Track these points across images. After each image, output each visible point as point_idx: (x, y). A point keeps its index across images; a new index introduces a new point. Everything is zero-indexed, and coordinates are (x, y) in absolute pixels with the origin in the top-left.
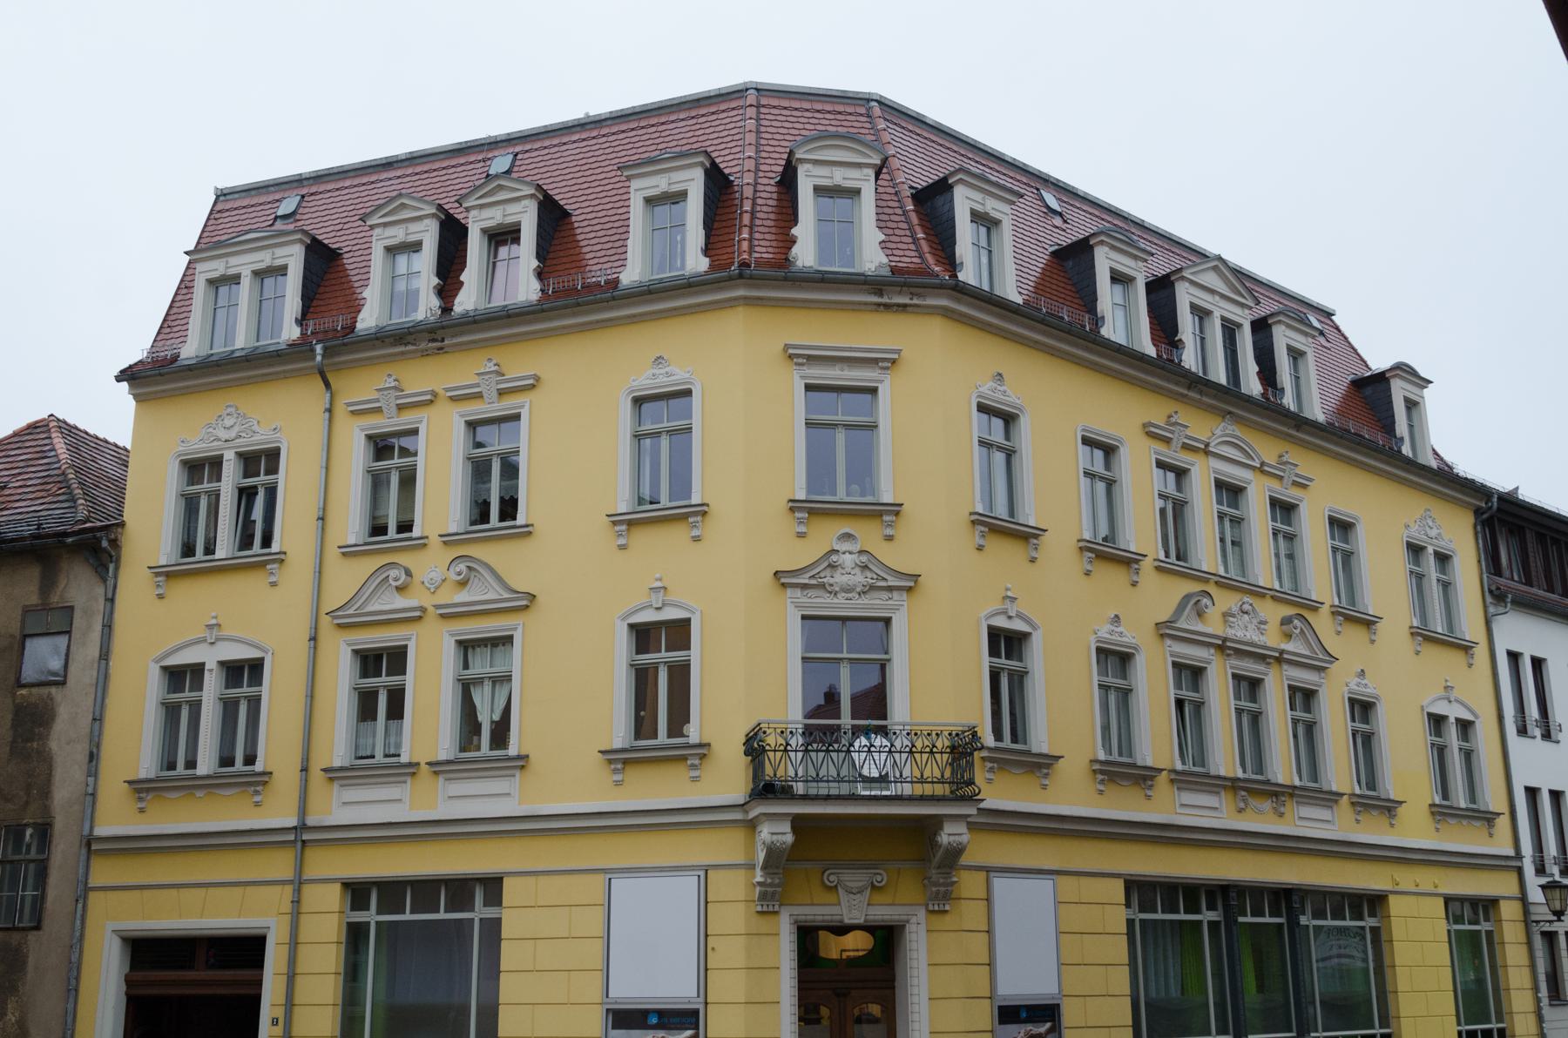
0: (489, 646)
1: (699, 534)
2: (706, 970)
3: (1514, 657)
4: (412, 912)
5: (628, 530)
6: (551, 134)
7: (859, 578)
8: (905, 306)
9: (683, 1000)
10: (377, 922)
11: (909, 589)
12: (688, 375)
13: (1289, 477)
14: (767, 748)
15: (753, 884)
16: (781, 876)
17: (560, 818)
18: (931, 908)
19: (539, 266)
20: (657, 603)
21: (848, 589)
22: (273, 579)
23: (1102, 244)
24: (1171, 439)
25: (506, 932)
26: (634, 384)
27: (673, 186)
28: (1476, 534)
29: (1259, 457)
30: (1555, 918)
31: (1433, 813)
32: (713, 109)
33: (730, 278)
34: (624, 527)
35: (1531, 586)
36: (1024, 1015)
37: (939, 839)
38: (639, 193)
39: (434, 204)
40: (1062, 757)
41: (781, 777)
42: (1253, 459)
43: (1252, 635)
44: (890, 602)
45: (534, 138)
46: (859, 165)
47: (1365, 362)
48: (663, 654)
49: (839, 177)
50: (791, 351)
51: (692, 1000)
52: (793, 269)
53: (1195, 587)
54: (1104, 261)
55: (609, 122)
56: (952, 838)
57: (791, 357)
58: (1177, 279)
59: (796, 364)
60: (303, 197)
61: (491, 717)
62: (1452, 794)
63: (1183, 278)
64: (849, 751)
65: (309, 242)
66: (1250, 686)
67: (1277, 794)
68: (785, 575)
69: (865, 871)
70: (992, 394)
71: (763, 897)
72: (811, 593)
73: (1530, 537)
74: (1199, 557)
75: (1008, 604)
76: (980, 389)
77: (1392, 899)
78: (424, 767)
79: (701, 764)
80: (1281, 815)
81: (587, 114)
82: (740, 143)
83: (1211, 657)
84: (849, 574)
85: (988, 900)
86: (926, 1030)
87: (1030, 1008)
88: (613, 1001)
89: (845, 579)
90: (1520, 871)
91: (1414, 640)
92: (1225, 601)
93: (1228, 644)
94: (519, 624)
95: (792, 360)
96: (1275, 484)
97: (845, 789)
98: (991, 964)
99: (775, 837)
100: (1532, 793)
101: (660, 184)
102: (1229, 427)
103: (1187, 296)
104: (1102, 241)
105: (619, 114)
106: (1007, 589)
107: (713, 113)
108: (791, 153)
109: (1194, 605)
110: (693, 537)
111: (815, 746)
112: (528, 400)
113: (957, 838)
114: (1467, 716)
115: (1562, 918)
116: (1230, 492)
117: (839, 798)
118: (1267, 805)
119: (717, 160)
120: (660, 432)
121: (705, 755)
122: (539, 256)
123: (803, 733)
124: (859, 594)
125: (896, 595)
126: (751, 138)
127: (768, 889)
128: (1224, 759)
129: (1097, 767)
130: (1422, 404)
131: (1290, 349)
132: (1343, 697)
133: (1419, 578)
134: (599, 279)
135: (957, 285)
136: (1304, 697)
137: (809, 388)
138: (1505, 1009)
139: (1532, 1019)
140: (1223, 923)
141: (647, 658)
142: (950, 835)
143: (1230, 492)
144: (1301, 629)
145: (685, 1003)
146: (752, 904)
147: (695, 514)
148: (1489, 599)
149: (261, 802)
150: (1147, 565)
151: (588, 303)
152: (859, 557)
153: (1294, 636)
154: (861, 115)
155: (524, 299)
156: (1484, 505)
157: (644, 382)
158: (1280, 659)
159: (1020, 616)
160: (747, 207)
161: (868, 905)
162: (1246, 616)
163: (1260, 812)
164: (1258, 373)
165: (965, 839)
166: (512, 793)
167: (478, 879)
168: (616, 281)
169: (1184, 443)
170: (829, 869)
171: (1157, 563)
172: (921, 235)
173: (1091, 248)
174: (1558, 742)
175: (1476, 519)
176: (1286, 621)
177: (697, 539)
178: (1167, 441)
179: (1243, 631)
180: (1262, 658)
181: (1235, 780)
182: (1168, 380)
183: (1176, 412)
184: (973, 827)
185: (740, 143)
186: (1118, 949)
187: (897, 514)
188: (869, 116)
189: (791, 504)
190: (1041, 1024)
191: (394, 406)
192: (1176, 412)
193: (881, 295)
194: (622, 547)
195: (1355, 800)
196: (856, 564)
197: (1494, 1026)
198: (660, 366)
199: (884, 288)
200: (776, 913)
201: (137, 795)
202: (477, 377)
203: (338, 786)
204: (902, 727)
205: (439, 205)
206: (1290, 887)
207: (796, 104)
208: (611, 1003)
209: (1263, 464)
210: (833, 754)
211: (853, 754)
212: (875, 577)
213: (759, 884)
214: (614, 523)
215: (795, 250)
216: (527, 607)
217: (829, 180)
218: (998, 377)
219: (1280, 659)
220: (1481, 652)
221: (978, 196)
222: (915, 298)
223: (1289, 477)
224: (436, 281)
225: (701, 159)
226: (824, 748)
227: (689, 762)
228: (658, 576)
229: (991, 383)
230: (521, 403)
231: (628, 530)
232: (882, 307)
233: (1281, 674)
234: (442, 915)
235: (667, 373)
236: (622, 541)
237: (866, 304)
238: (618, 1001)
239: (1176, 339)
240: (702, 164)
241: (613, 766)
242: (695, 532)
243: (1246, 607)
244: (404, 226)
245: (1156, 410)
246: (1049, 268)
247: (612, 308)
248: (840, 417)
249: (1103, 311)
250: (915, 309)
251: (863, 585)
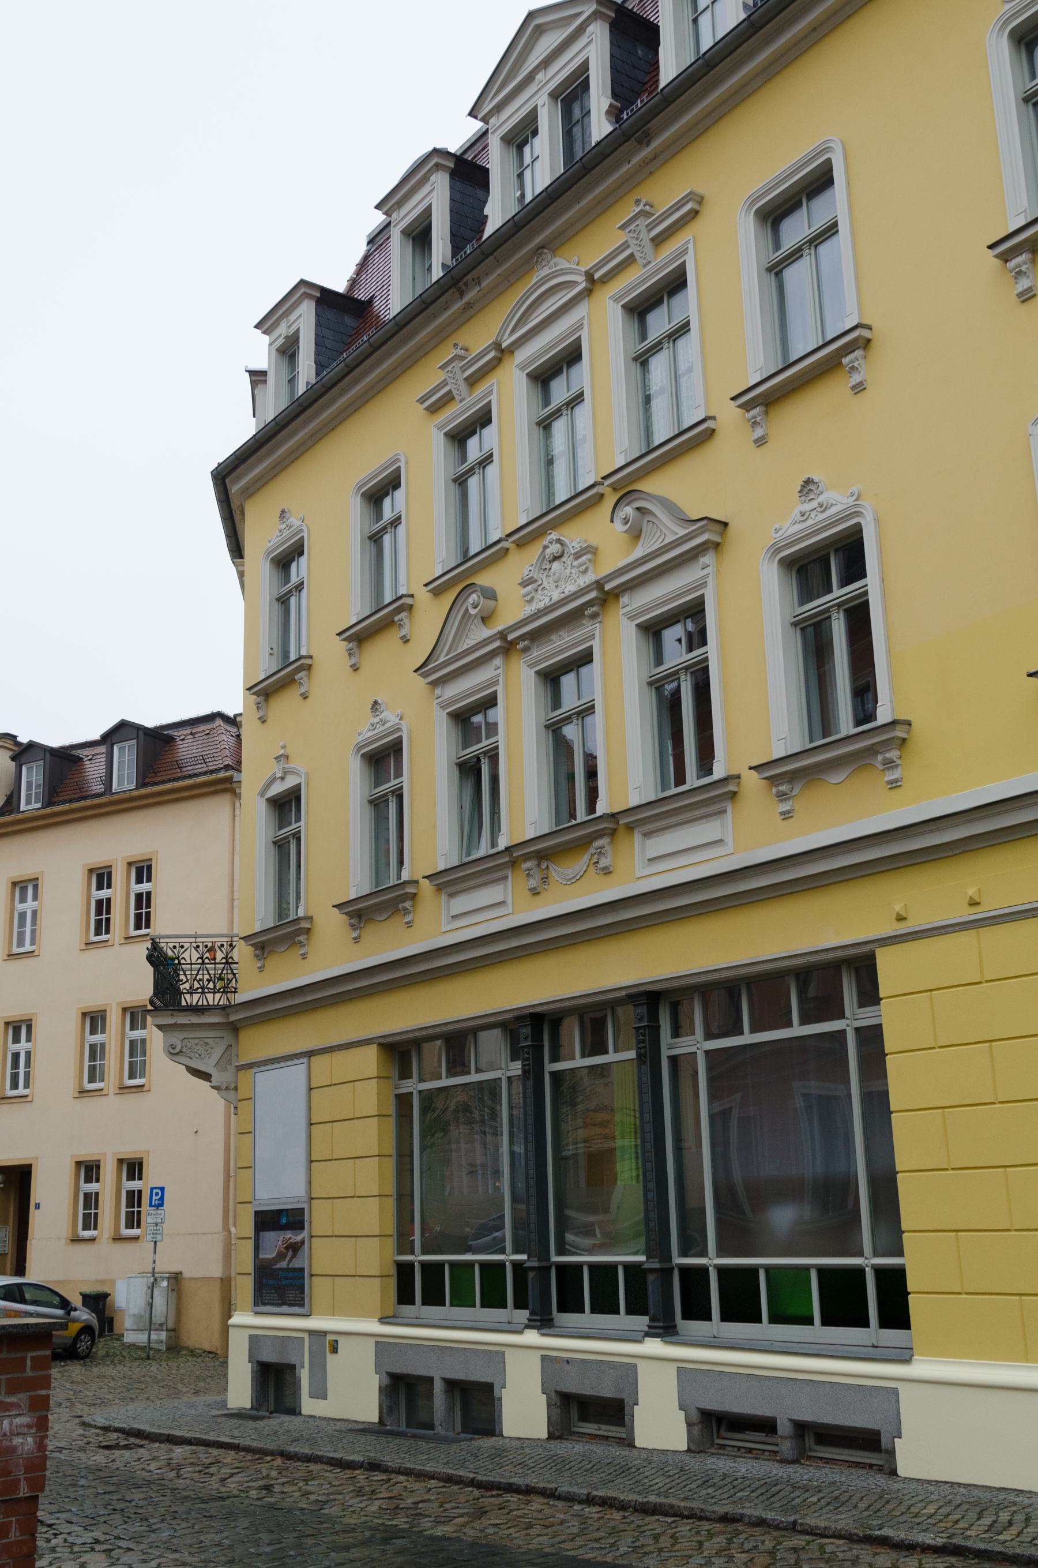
1: (1030, 284)
4: (754, 1030)
5: (766, 413)
9: (293, 1200)
10: (707, 1052)
22: (856, 378)
25: (890, 1042)
65: (318, 295)
78: (752, 781)
197: (868, 1261)
201: (774, 790)
203: (640, 836)
231: (766, 413)
234: (798, 1030)
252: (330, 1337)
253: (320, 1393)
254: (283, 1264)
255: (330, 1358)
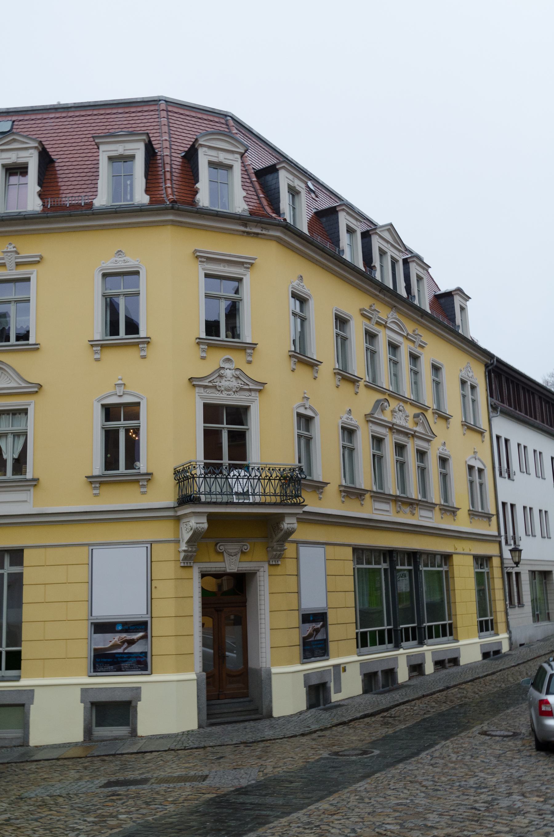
0: (11, 415)
2: (152, 599)
3: (498, 438)
6: (36, 112)
7: (234, 384)
8: (257, 234)
11: (260, 391)
12: (137, 263)
13: (418, 342)
14: (195, 476)
15: (179, 551)
16: (196, 547)
17: (64, 515)
18: (271, 563)
19: (40, 191)
20: (120, 392)
21: (228, 389)
23: (343, 211)
24: (371, 318)
25: (26, 580)
26: (104, 265)
27: (19, 159)
28: (486, 376)
29: (406, 330)
30: (515, 565)
31: (469, 514)
32: (139, 109)
33: (166, 209)
34: (99, 348)
35: (504, 404)
36: (311, 618)
37: (282, 526)
38: (105, 153)
39: (38, 141)
40: (329, 483)
41: (203, 492)
42: (404, 331)
43: (402, 423)
44: (250, 397)
45: (25, 113)
46: (233, 152)
47: (437, 286)
48: (122, 422)
49: (222, 157)
50: (198, 254)
51: (143, 616)
52: (198, 207)
53: (381, 397)
54: (343, 220)
55: (73, 109)
56: (289, 526)
57: (197, 257)
58: (373, 234)
59: (200, 261)
60: (14, 122)
61: (13, 456)
62: (476, 505)
63: (376, 233)
64: (227, 478)
66: (400, 448)
67: (412, 504)
68: (195, 380)
69: (238, 543)
70: (297, 286)
71: (185, 558)
72: (208, 390)
73: (503, 379)
74: (382, 380)
75: (305, 401)
76: (293, 284)
77: (455, 557)
79: (147, 485)
80: (413, 514)
81: (59, 102)
82: (158, 131)
83: (387, 433)
84: (229, 382)
85: (297, 558)
86: (268, 628)
87: (124, 624)
88: (95, 618)
89: (227, 383)
90: (500, 543)
91: (463, 428)
92: (394, 404)
93: (395, 427)
94: (32, 402)
95: (198, 259)
96: (411, 345)
97: (225, 499)
98: (298, 593)
99: (198, 525)
100: (504, 504)
101: (119, 149)
102: (395, 314)
103: (378, 243)
104: (344, 209)
105: (80, 105)
106: (305, 393)
107: (139, 112)
108: (196, 140)
109: (379, 405)
110: (141, 356)
111: (209, 475)
112: (36, 270)
113: (291, 525)
114: (482, 467)
115: (519, 565)
116: (394, 347)
117: (221, 504)
118: (408, 509)
119: (152, 139)
120: (119, 295)
121: (150, 479)
122: (40, 184)
123: (204, 467)
124: (234, 392)
125: (253, 394)
126: (165, 129)
127: (189, 554)
128: (392, 488)
129: (342, 489)
130: (466, 309)
131: (418, 276)
132: (437, 456)
133: (464, 396)
134: (80, 202)
135: (287, 225)
136: (421, 454)
137: (207, 276)
138: (453, 612)
139: (503, 614)
140: (389, 570)
141: (112, 424)
142: (288, 523)
143: (394, 347)
144: (423, 421)
145: (139, 618)
146: (178, 562)
147: (143, 343)
148: (490, 409)
149: (146, 492)
150: (362, 383)
151: (52, 217)
152: (235, 372)
153: (419, 424)
154: (223, 124)
155: (32, 209)
156: (489, 362)
157: (109, 265)
158: (414, 435)
159: (311, 408)
160: (168, 169)
161: (239, 562)
162: (400, 412)
163: (405, 513)
164: (405, 287)
165: (295, 526)
166: (28, 500)
167: (6, 551)
168: (91, 204)
169: (377, 321)
170: (219, 543)
171: (366, 383)
172: (262, 196)
173: (337, 212)
174: (513, 480)
175: (485, 369)
176: (416, 416)
177: (144, 357)
178: (369, 319)
179: (399, 420)
180: (406, 434)
181: (397, 496)
182: (371, 287)
183: (374, 304)
184: (300, 521)
185: (158, 131)
186: (349, 583)
187: (253, 349)
188: (227, 125)
189: (198, 340)
190: (319, 623)
191: (14, 263)
192: (374, 304)
193: (246, 227)
194: (97, 360)
195: (442, 507)
196: (233, 376)
197: (447, 622)
198: (120, 256)
199: (248, 223)
200: (191, 567)
202: (2, 254)
204: (265, 466)
205: (41, 142)
206: (417, 551)
207: (187, 113)
208: (94, 619)
209: (408, 334)
210: (229, 480)
211: (240, 480)
212: (243, 383)
213: (185, 551)
214: (92, 346)
215: (198, 197)
216: (37, 392)
217: (217, 159)
218: (300, 278)
219: (414, 435)
220: (487, 434)
221: (291, 177)
222: (264, 230)
223: (418, 342)
224: (38, 189)
225: (144, 137)
226: (214, 476)
227: (141, 483)
228: (120, 377)
229: (297, 281)
230: (33, 272)
232: (245, 234)
233: (414, 443)
235: (124, 261)
236: (97, 356)
237: (237, 231)
238: (98, 618)
239: (372, 265)
240: (144, 140)
241: (93, 486)
242: (143, 353)
243: (401, 408)
244: (16, 152)
245: (365, 302)
246: (312, 219)
247: (90, 220)
248: (222, 293)
249: (343, 247)
250: (263, 237)
251: (237, 388)
252: (342, 666)
253: (338, 690)
254: (312, 639)
255: (343, 675)
